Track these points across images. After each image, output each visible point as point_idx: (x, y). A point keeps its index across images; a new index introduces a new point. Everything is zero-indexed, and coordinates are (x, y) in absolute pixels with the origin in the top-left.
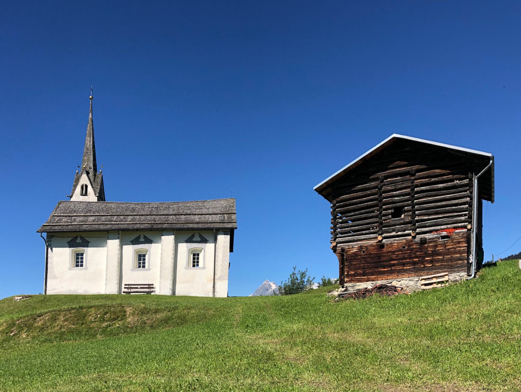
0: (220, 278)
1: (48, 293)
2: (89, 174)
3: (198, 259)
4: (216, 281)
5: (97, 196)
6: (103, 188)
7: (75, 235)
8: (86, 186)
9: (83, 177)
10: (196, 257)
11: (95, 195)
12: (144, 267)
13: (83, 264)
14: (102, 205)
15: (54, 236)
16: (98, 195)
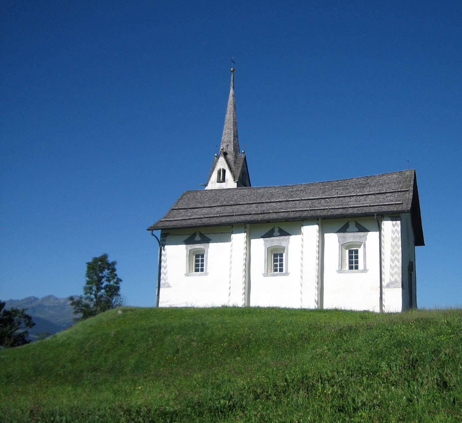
0: (388, 286)
1: (161, 305)
2: (227, 155)
3: (357, 257)
4: (384, 290)
5: (237, 182)
6: (247, 172)
7: (192, 231)
8: (224, 171)
9: (220, 161)
10: (200, 259)
11: (234, 180)
12: (281, 270)
13: (282, 269)
14: (245, 191)
15: (169, 233)
16: (237, 181)
